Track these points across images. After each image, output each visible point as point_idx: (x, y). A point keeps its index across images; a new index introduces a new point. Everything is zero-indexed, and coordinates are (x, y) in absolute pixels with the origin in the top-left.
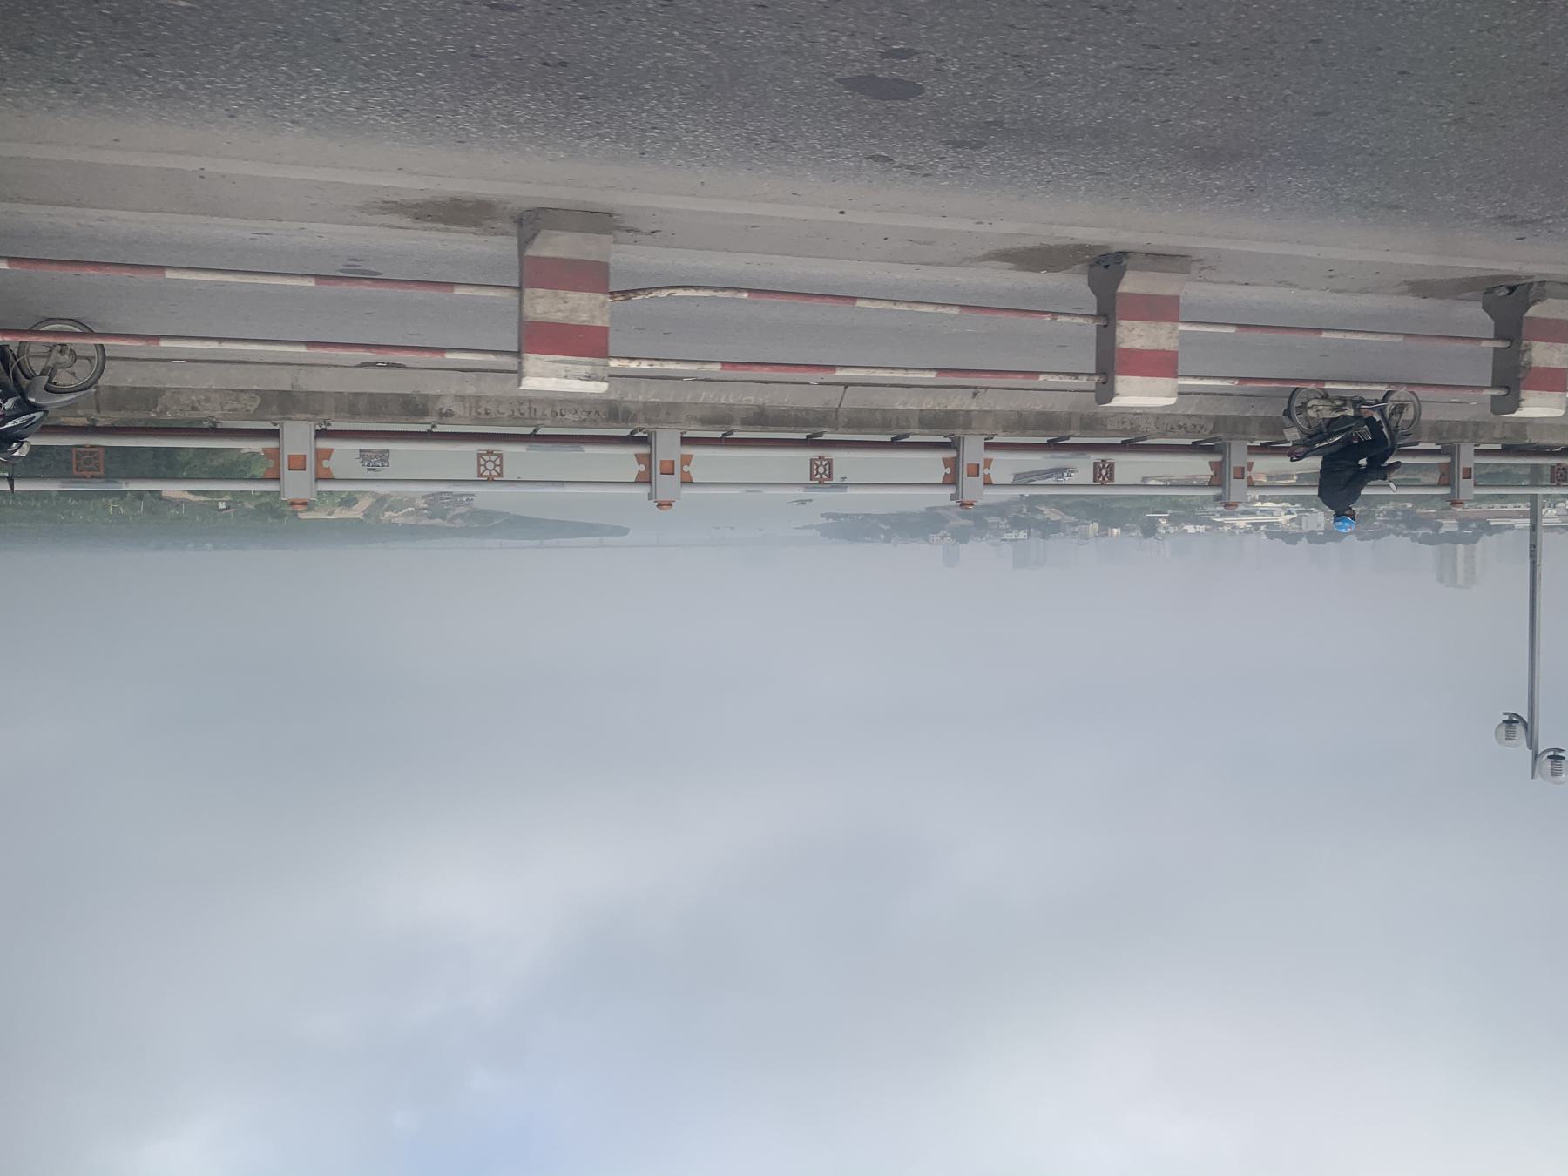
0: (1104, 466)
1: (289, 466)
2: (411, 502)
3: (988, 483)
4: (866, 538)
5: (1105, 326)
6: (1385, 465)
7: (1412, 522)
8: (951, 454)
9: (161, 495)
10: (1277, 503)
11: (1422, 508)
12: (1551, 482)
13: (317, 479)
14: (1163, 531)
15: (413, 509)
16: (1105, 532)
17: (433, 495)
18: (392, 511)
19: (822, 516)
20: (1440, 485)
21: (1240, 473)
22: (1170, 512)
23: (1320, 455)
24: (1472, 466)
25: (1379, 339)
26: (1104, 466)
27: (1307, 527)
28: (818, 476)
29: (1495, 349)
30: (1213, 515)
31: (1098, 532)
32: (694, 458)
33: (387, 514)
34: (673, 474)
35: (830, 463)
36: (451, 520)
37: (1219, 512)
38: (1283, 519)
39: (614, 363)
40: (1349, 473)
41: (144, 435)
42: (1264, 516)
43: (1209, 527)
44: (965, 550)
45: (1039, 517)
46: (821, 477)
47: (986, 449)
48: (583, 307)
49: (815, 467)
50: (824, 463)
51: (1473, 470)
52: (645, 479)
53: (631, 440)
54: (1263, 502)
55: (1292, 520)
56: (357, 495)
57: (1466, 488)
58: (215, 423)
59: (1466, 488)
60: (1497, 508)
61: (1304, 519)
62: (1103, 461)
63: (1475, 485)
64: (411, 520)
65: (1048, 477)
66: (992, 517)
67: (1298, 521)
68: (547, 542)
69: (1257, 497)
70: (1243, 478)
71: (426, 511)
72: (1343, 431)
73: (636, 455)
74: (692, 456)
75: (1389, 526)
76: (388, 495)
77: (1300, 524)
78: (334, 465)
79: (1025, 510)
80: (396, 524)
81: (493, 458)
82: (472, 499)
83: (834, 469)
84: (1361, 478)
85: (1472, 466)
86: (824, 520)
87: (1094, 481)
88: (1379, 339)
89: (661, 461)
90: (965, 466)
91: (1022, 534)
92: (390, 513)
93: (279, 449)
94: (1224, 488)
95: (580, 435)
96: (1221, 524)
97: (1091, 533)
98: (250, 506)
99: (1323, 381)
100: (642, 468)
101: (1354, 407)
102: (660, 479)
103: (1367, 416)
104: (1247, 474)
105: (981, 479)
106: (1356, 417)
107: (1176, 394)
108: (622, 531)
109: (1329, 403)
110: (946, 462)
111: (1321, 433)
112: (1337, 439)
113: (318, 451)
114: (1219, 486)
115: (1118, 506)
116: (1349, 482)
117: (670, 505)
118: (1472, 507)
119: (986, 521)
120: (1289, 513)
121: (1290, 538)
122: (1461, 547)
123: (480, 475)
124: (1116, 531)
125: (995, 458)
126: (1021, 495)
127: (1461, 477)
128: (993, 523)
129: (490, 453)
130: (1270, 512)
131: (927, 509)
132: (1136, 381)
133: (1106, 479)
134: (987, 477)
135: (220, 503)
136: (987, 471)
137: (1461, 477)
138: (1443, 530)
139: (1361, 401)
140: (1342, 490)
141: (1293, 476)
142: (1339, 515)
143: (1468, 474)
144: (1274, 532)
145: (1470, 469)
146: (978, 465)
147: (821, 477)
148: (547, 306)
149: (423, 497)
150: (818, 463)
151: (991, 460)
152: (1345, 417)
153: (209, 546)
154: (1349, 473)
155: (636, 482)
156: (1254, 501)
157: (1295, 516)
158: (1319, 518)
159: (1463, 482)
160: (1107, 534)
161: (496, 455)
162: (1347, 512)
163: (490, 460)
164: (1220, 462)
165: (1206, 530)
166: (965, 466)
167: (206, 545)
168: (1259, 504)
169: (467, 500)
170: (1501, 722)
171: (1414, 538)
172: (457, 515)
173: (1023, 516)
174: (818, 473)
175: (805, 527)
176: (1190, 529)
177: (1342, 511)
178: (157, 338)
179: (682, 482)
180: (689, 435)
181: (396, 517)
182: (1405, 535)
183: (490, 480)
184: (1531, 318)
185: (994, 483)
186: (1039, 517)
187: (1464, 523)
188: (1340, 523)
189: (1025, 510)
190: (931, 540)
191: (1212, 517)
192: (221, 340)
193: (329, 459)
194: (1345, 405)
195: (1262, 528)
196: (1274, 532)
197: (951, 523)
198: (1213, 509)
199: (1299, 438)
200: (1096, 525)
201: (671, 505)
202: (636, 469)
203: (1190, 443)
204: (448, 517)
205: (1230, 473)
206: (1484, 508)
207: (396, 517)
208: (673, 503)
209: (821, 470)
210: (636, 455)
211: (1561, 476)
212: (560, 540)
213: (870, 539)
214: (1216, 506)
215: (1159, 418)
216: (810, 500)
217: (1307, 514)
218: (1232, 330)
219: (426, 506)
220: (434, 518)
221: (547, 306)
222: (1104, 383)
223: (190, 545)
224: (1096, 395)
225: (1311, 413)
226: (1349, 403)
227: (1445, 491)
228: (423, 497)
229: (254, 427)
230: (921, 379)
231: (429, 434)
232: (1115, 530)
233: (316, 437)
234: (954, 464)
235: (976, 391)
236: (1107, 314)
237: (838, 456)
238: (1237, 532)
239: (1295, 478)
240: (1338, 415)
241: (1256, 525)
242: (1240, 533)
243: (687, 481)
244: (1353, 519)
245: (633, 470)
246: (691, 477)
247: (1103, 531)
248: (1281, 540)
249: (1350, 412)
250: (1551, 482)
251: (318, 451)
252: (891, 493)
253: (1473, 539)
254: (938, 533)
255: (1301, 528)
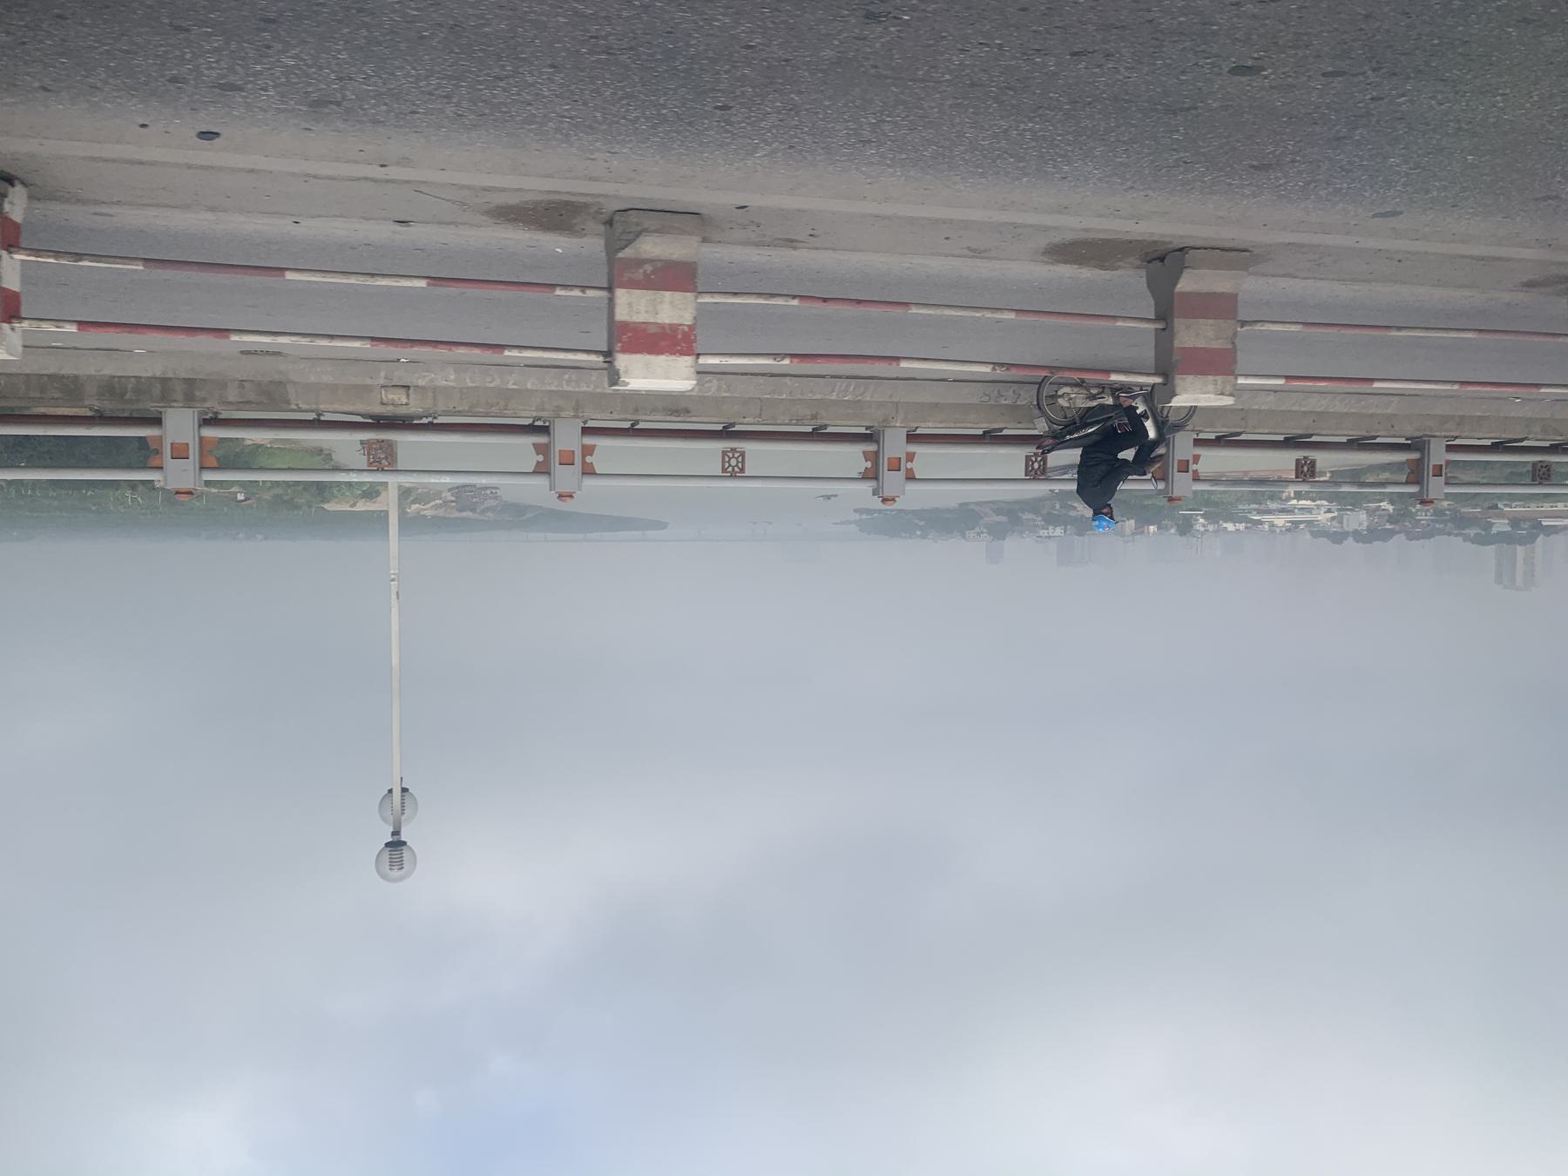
0: (1306, 462)
1: (172, 454)
2: (438, 495)
3: (911, 477)
4: (903, 535)
5: (1164, 329)
6: (1152, 456)
7: (1460, 522)
8: (872, 448)
9: (154, 485)
10: (1314, 501)
11: (1244, 505)
12: (1533, 480)
13: (202, 468)
14: (1202, 529)
15: (441, 502)
16: (1141, 530)
17: (457, 488)
18: (420, 504)
19: (856, 511)
20: (1407, 483)
21: (1184, 467)
22: (1204, 509)
23: (1080, 447)
24: (1443, 463)
25: (959, 314)
26: (1306, 462)
27: (1348, 526)
28: (730, 469)
29: (1156, 329)
30: (1250, 513)
31: (1135, 529)
32: (597, 448)
33: (415, 507)
34: (573, 464)
35: (743, 454)
36: (483, 512)
37: (1255, 510)
38: (1322, 517)
39: (1241, 381)
40: (1103, 468)
41: (71, 423)
42: (1303, 514)
43: (1249, 525)
44: (1011, 544)
45: (1072, 513)
46: (733, 469)
47: (1447, 451)
48: (672, 309)
49: (727, 459)
50: (736, 455)
51: (1444, 467)
52: (871, 475)
53: (531, 429)
54: (1298, 500)
55: (1333, 519)
56: (379, 488)
57: (1436, 487)
58: (216, 413)
59: (1436, 487)
60: (1547, 507)
61: (1345, 517)
62: (1305, 457)
63: (1447, 483)
64: (440, 512)
65: (1065, 474)
66: (1026, 513)
67: (1339, 519)
68: (589, 535)
69: (1292, 495)
70: (1188, 472)
71: (453, 504)
72: (1097, 422)
73: (534, 444)
74: (595, 446)
75: (1437, 526)
76: (413, 488)
77: (1341, 523)
78: (598, 462)
79: (1058, 506)
80: (425, 516)
81: (736, 455)
82: (496, 493)
83: (746, 462)
84: (1121, 470)
85: (1443, 463)
86: (857, 516)
87: (1026, 475)
88: (959, 314)
89: (889, 458)
90: (886, 459)
91: (1059, 531)
92: (417, 505)
93: (161, 437)
94: (1167, 483)
95: (294, 420)
96: (1260, 522)
97: (1128, 531)
98: (267, 496)
99: (1108, 372)
100: (869, 464)
101: (1113, 395)
102: (558, 470)
103: (1126, 404)
104: (1193, 467)
105: (902, 474)
106: (1117, 406)
107: (694, 376)
108: (662, 526)
109: (1085, 392)
110: (866, 455)
111: (1075, 423)
112: (1090, 431)
113: (584, 447)
114: (1417, 483)
115: (1150, 503)
116: (1104, 477)
117: (571, 496)
118: (1520, 506)
119: (1021, 517)
120: (1329, 511)
121: (1338, 537)
122: (1520, 550)
123: (724, 470)
124: (1152, 528)
125: (399, 440)
126: (1050, 490)
127: (1431, 474)
128: (1028, 520)
129: (734, 450)
130: (1309, 510)
131: (961, 505)
132: (1198, 381)
133: (1039, 473)
134: (1195, 472)
135: (239, 494)
136: (909, 465)
137: (1175, 470)
138: (1494, 530)
139: (1122, 389)
140: (1097, 486)
141: (1325, 473)
142: (1097, 513)
143: (1438, 471)
144: (1318, 532)
145: (1441, 466)
146: (1188, 461)
147: (733, 469)
148: (634, 306)
149: (449, 490)
150: (1034, 459)
151: (914, 454)
152: (1102, 407)
153: (260, 537)
154: (1103, 468)
155: (534, 472)
156: (1289, 499)
157: (1336, 514)
158: (1361, 516)
159: (1178, 476)
160: (1143, 532)
161: (739, 452)
162: (1105, 511)
163: (733, 457)
164: (1418, 460)
165: (1246, 528)
166: (886, 459)
167: (257, 535)
168: (1294, 502)
169: (492, 493)
170: (383, 846)
171: (1467, 538)
172: (487, 508)
173: (1056, 512)
174: (730, 465)
175: (842, 523)
176: (1230, 527)
177: (1102, 509)
178: (501, 347)
179: (583, 473)
180: (590, 424)
181: (425, 510)
182: (1456, 535)
183: (733, 476)
184: (1182, 294)
185: (917, 477)
186: (1072, 513)
187: (1515, 522)
188: (1097, 523)
189: (1058, 506)
190: (967, 537)
191: (1248, 515)
192: (332, 337)
193: (591, 455)
194: (1103, 392)
195: (1302, 526)
196: (1318, 532)
197: (985, 519)
198: (1246, 507)
199: (1047, 429)
200: (1132, 522)
201: (895, 501)
202: (533, 459)
203: (1490, 444)
204: (478, 511)
205: (884, 465)
206: (1533, 507)
207: (425, 510)
208: (897, 499)
209: (733, 462)
210: (534, 444)
211: (1544, 474)
212: (603, 534)
213: (907, 535)
214: (1249, 505)
215: (672, 403)
216: (836, 496)
217: (1349, 513)
218: (422, 283)
219: (453, 499)
220: (464, 511)
221: (634, 306)
222: (1165, 384)
223: (240, 535)
224: (609, 373)
225: (1062, 402)
226: (1107, 390)
227: (1413, 489)
228: (449, 490)
229: (300, 418)
230: (543, 359)
231: (316, 422)
232: (1152, 527)
233: (200, 426)
234: (874, 458)
235: (459, 366)
236: (1164, 315)
237: (749, 447)
238: (1278, 530)
239: (1328, 475)
240: (1094, 403)
241: (1296, 524)
242: (1281, 531)
243: (911, 477)
244: (1111, 518)
245: (531, 460)
246: (594, 470)
247: (1139, 530)
248: (1326, 539)
249: (1110, 401)
250: (1533, 480)
251: (584, 447)
252: (788, 486)
253: (1531, 539)
254: (973, 529)
255: (1342, 527)
